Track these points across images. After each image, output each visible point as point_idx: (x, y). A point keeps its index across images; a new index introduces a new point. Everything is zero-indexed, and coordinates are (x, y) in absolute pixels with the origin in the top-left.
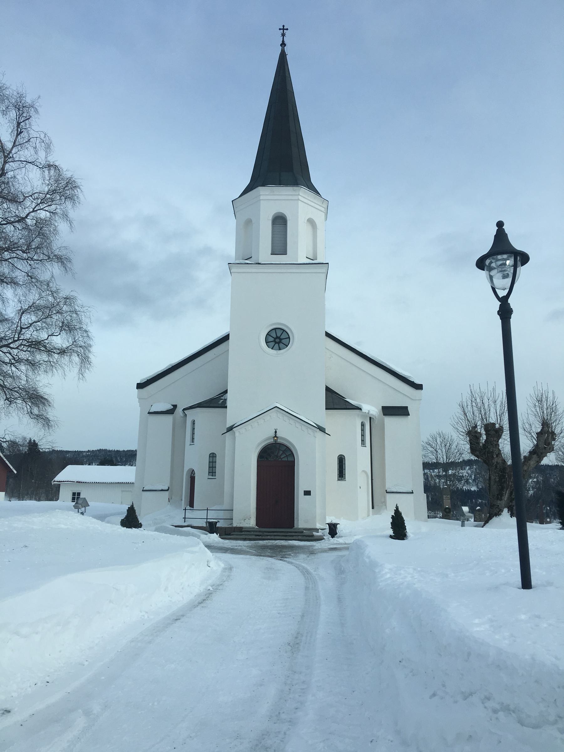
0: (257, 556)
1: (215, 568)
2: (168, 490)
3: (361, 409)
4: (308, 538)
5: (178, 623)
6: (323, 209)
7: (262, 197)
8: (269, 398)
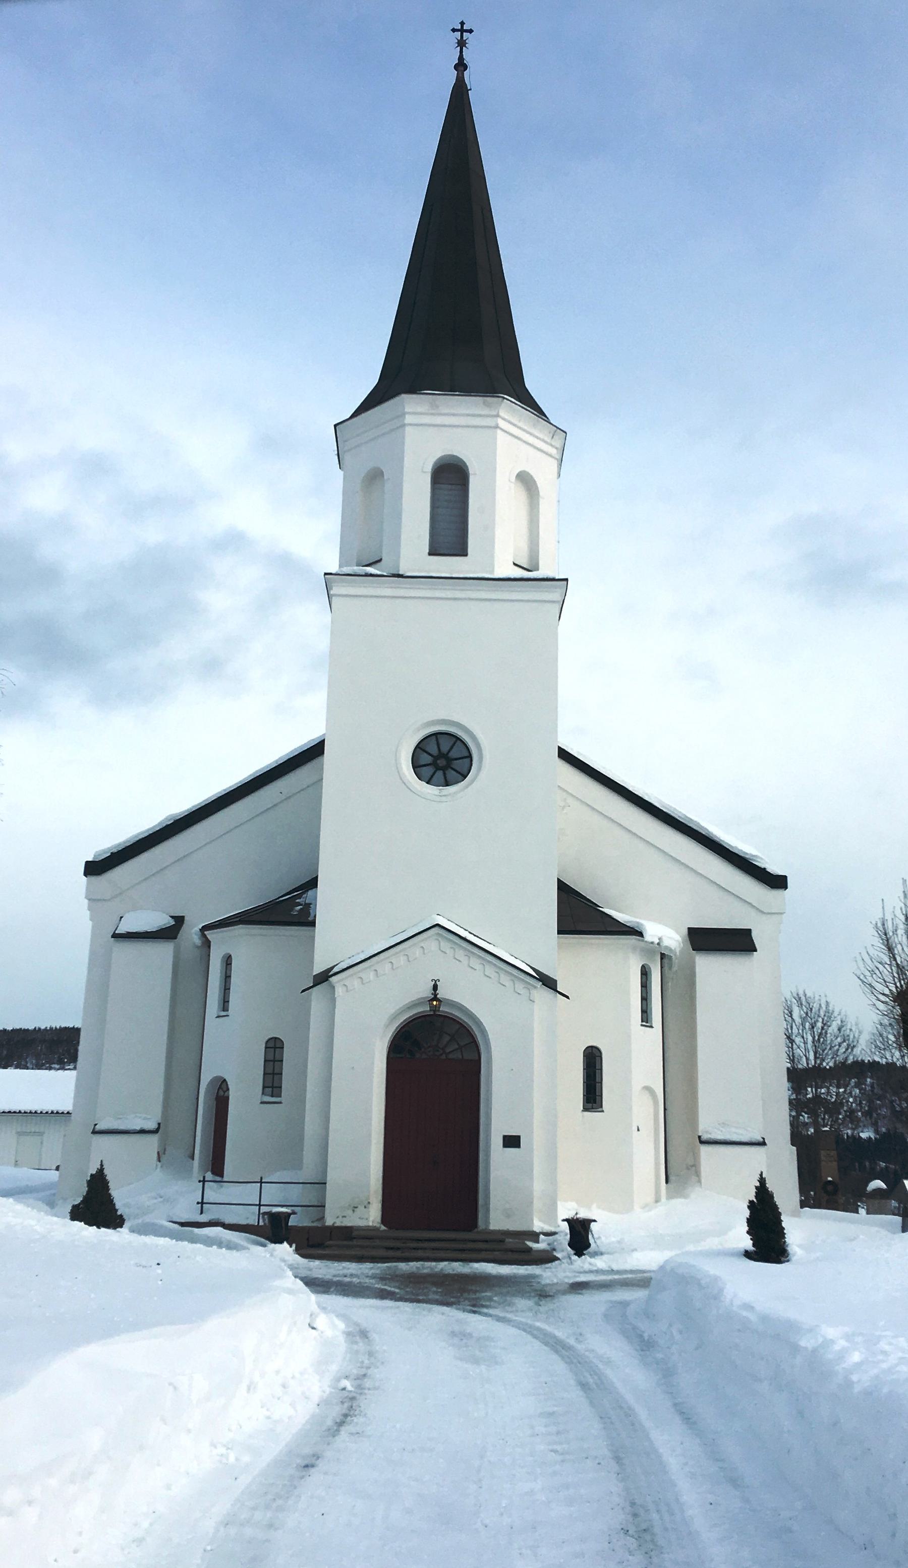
0: (412, 1301)
1: (329, 1333)
2: (155, 1131)
3: (640, 934)
4: (516, 1256)
5: (315, 1476)
6: (553, 451)
7: (409, 419)
8: (417, 899)
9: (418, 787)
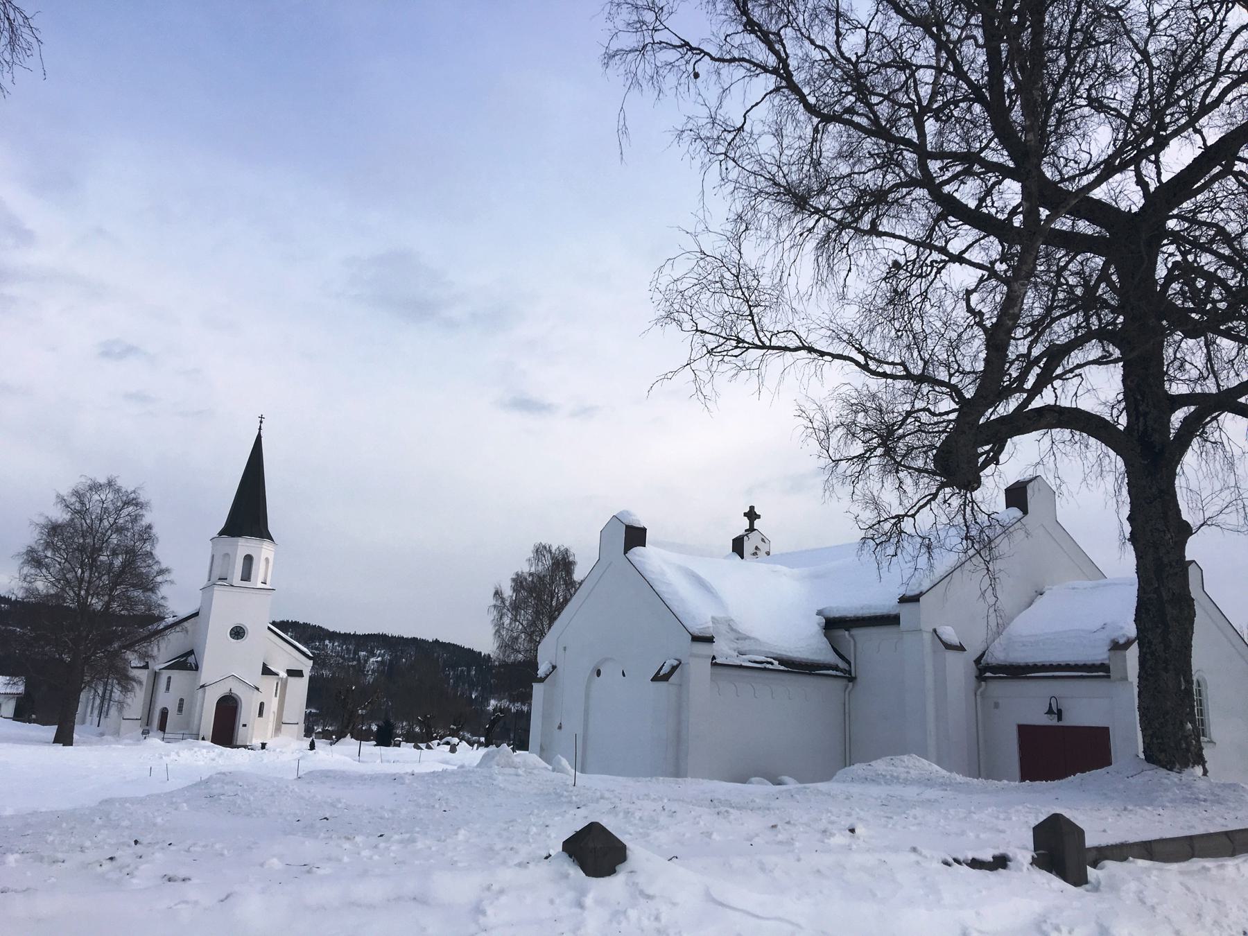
9: (337, 756)
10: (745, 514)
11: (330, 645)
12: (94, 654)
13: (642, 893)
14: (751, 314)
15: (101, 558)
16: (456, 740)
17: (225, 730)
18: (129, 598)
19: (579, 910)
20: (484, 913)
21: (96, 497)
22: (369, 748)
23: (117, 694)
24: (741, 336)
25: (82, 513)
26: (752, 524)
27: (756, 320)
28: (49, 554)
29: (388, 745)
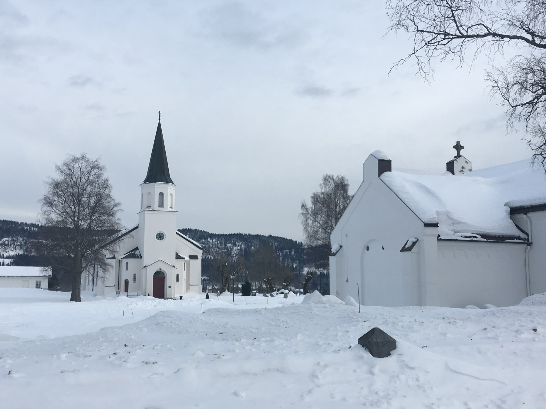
10: (454, 147)
11: (211, 241)
12: (86, 252)
13: (407, 366)
14: (453, 16)
15: (83, 199)
16: (286, 291)
17: (160, 289)
18: (100, 220)
19: (370, 376)
20: (317, 377)
21: (76, 166)
22: (239, 297)
23: (100, 273)
24: (447, 31)
25: (70, 175)
26: (458, 153)
27: (457, 19)
28: (56, 199)
29: (249, 295)
